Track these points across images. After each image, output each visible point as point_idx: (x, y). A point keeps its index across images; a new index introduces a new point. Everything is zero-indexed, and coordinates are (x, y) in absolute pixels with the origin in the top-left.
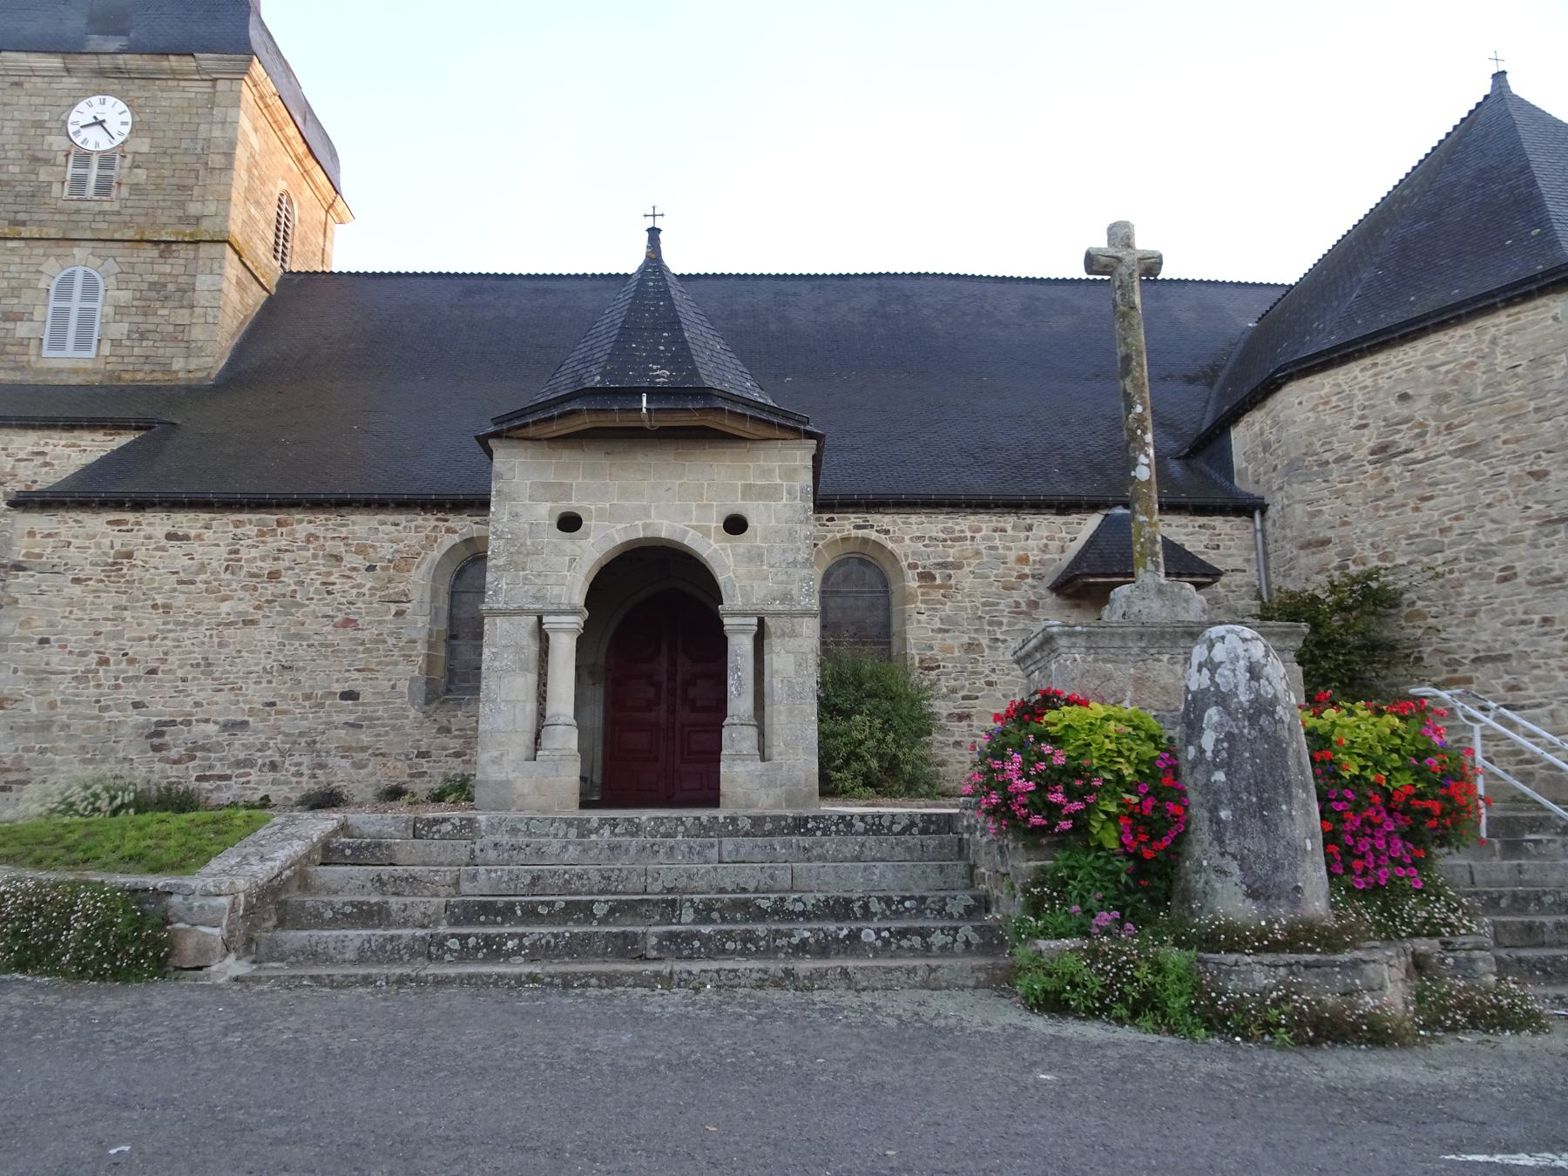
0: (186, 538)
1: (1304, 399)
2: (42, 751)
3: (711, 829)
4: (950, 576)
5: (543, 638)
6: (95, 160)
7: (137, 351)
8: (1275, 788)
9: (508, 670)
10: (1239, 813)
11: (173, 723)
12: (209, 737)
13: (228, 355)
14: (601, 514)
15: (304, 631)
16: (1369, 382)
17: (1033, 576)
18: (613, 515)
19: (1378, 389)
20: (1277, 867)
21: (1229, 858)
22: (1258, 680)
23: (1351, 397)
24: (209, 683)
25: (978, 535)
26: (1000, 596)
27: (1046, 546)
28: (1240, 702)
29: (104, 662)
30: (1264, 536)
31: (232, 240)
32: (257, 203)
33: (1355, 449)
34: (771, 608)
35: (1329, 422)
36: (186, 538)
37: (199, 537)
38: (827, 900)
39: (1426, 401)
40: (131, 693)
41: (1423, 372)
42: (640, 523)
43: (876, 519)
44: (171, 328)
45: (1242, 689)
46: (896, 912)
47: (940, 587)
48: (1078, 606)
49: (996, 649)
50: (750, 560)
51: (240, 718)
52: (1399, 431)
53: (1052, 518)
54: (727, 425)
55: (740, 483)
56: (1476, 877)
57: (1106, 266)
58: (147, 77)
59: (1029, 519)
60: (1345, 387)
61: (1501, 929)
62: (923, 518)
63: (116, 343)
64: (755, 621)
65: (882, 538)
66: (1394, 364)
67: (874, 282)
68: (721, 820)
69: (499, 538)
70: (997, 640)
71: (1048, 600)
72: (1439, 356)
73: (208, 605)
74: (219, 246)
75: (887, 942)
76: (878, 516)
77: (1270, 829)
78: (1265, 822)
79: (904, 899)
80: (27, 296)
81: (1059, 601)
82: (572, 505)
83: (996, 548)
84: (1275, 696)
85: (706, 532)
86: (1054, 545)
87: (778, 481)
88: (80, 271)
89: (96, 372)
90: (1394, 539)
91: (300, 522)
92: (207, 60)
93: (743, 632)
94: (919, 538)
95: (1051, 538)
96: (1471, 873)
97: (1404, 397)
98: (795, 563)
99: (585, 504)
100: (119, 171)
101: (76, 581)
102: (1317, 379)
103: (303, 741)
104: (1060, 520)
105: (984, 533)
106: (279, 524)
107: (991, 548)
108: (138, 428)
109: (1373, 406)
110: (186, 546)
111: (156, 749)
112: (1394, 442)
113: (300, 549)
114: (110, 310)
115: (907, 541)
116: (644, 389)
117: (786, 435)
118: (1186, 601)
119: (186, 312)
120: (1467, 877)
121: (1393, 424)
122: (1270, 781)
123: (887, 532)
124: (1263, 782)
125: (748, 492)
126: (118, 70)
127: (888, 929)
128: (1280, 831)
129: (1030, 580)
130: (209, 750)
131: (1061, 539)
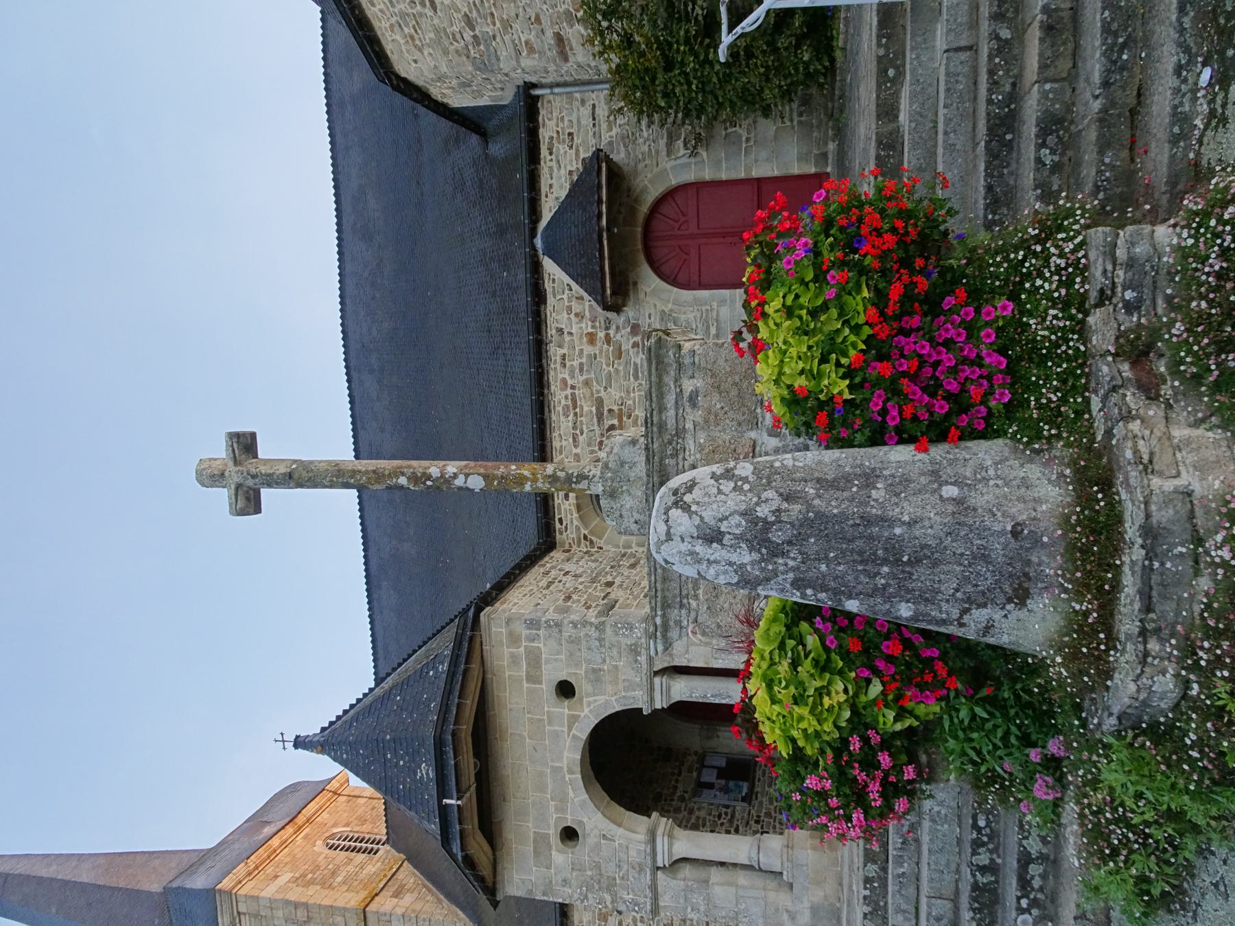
3: (877, 903)
4: (610, 411)
8: (871, 538)
9: (708, 899)
10: (904, 592)
13: (454, 907)
14: (561, 809)
17: (607, 328)
18: (562, 799)
20: (983, 556)
21: (966, 618)
22: (722, 534)
23: (403, 15)
25: (570, 382)
26: (628, 363)
27: (577, 315)
28: (753, 563)
30: (558, 85)
31: (363, 905)
32: (334, 874)
34: (645, 666)
35: (432, 35)
38: (974, 910)
45: (734, 557)
46: (991, 837)
48: (635, 284)
50: (598, 680)
53: (549, 308)
54: (470, 704)
55: (526, 685)
56: (963, 43)
57: (248, 499)
59: (551, 332)
60: (393, 20)
61: (1050, 73)
64: (657, 680)
67: (354, 374)
68: (867, 893)
69: (586, 897)
74: (368, 915)
75: (1034, 903)
77: (926, 556)
78: (918, 561)
79: (975, 826)
81: (631, 303)
82: (553, 834)
83: (581, 364)
84: (743, 514)
85: (573, 720)
86: (576, 307)
87: (522, 649)
93: (669, 690)
94: (574, 440)
96: (958, 49)
98: (600, 640)
99: (552, 822)
102: (389, 47)
104: (551, 300)
107: (581, 370)
116: (440, 801)
117: (478, 644)
118: (622, 464)
120: (963, 56)
122: (859, 543)
124: (861, 553)
125: (533, 678)
127: (1019, 899)
128: (933, 543)
129: (612, 332)
131: (570, 300)
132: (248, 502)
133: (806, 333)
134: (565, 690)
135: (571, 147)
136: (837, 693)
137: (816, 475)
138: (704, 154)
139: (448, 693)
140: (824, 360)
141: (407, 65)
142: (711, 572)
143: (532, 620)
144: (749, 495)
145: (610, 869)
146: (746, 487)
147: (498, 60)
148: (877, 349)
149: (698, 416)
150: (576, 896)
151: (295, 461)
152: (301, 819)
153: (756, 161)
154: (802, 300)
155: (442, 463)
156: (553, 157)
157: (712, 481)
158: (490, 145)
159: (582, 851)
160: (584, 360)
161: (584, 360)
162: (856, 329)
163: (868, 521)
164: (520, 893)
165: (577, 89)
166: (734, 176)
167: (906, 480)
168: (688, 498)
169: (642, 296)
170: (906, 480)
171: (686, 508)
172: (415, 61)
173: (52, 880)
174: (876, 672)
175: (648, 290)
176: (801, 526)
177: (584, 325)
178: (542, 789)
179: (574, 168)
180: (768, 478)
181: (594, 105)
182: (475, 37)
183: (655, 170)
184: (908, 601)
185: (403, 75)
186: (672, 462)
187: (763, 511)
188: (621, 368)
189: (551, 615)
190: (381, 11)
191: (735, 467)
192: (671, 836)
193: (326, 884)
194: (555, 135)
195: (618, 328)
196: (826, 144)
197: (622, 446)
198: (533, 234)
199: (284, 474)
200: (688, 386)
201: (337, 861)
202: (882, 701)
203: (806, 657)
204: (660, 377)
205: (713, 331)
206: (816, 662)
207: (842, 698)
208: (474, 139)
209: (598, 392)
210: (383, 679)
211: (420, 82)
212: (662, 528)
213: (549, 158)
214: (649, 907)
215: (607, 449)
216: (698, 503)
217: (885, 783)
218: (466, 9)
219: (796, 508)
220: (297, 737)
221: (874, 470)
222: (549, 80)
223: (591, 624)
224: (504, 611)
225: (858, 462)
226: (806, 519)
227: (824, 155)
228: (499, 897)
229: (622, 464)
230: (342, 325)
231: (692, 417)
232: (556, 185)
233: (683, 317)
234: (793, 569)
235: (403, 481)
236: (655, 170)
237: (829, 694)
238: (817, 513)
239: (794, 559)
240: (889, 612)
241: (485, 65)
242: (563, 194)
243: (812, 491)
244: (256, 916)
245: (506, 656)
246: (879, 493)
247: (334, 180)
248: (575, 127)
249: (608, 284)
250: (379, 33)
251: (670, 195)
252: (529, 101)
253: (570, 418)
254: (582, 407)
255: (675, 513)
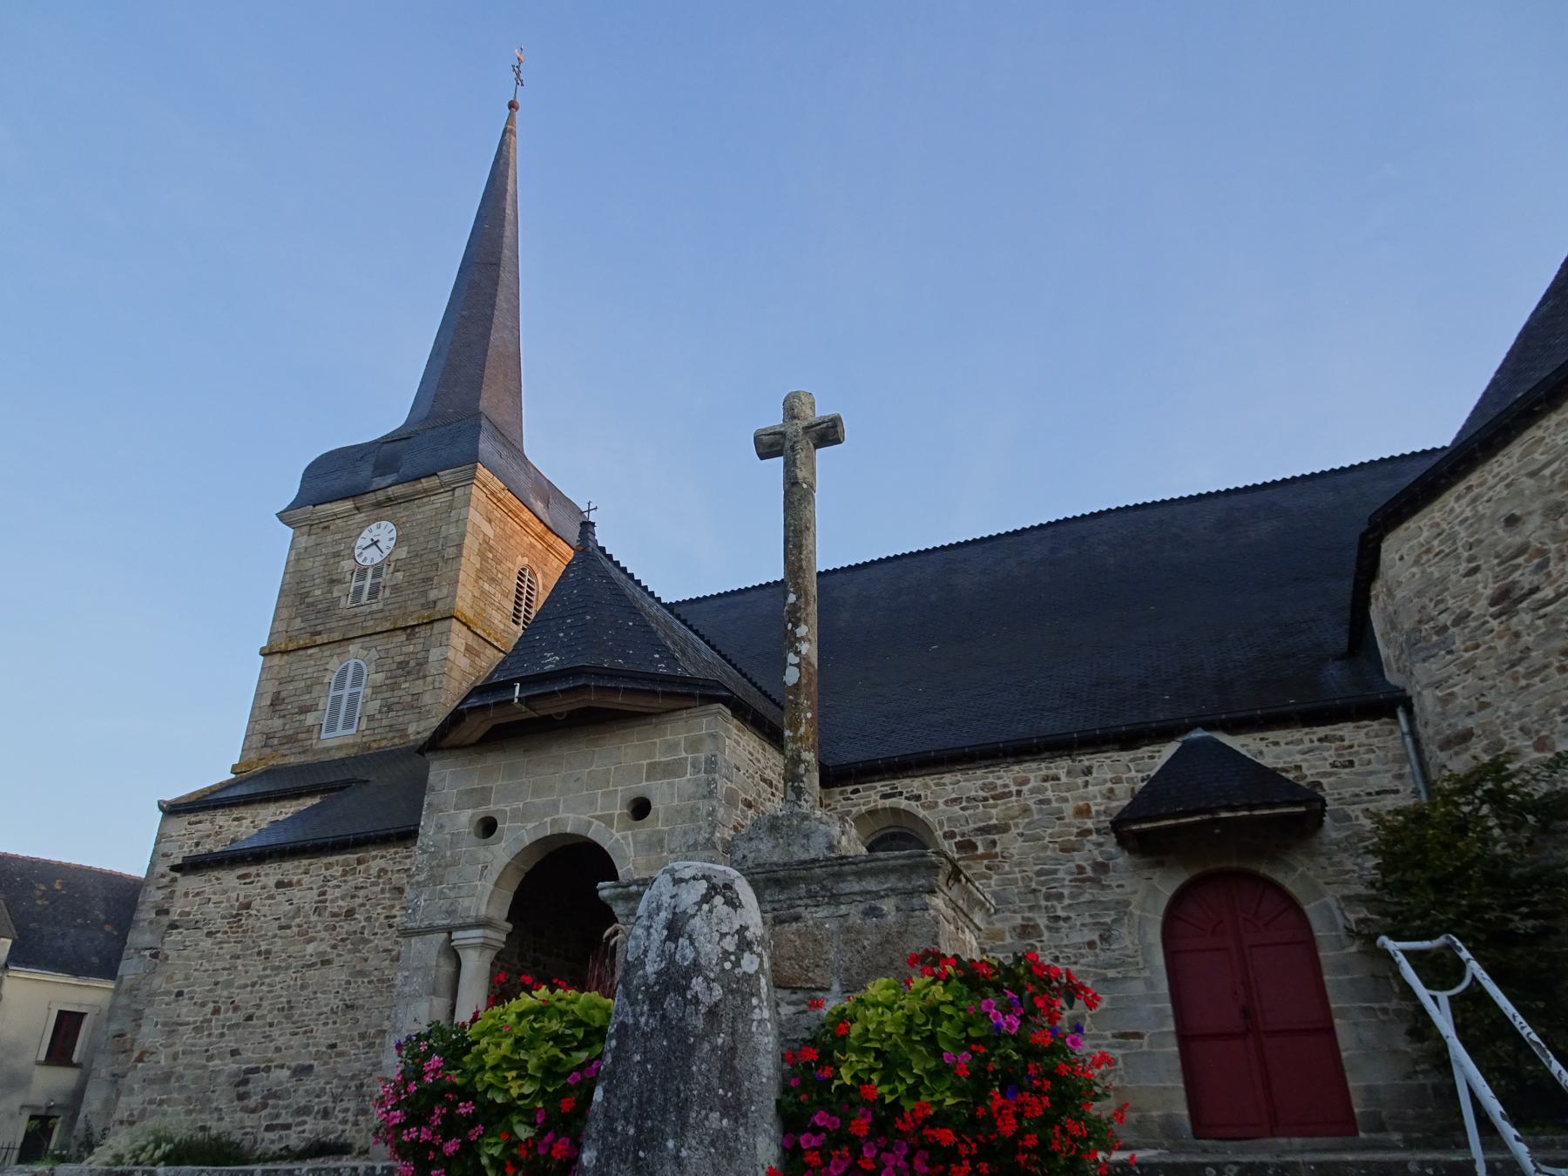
0: (290, 884)
1: (1404, 551)
2: (161, 1102)
4: (994, 843)
5: (453, 955)
6: (370, 572)
7: (385, 722)
8: (664, 1110)
9: (415, 996)
11: (256, 1070)
12: (280, 1083)
15: (368, 967)
16: (1468, 513)
18: (522, 816)
19: (1480, 518)
22: (676, 941)
23: (1453, 537)
24: (288, 1027)
25: (1025, 788)
27: (1111, 790)
28: (645, 976)
29: (216, 1011)
32: (493, 580)
33: (1473, 603)
35: (1437, 575)
36: (290, 884)
37: (299, 882)
39: (1536, 520)
40: (230, 1042)
41: (1528, 483)
42: (548, 820)
43: (914, 784)
44: (409, 698)
45: (651, 955)
47: (983, 857)
48: (1160, 864)
49: (1058, 930)
51: (307, 1063)
52: (1517, 567)
53: (1115, 755)
54: (619, 702)
57: (772, 445)
58: (408, 499)
59: (1086, 761)
60: (1444, 526)
62: (959, 776)
63: (371, 718)
65: (913, 806)
66: (1491, 481)
67: (1050, 531)
69: (425, 852)
70: (1057, 918)
71: (1120, 860)
72: (1539, 457)
73: (297, 948)
74: (447, 622)
76: (907, 781)
80: (317, 690)
82: (490, 809)
83: (1048, 801)
84: (695, 963)
85: (608, 820)
87: (684, 755)
88: (352, 662)
89: (354, 745)
90: (1546, 717)
91: (374, 858)
92: (446, 475)
95: (1117, 780)
97: (1512, 521)
99: (501, 806)
100: (386, 576)
101: (209, 934)
102: (1411, 524)
103: (353, 1084)
104: (1126, 756)
105: (1032, 784)
106: (359, 862)
107: (1041, 802)
108: (322, 792)
109: (1480, 541)
110: (289, 892)
111: (241, 1097)
112: (1514, 583)
113: (373, 884)
114: (369, 691)
115: (942, 806)
116: (516, 680)
118: (807, 836)
119: (420, 682)
121: (1507, 560)
122: (660, 1099)
123: (918, 798)
124: (650, 1101)
125: (654, 771)
126: (389, 499)
129: (1094, 837)
130: (279, 1098)
132: (768, 446)
133: (908, 1032)
134: (641, 808)
135: (1333, 765)
136: (520, 1086)
137: (740, 1047)
138: (1353, 949)
139: (632, 676)
140: (879, 1054)
141: (1397, 551)
142: (639, 931)
143: (715, 763)
144: (717, 969)
145: (452, 878)
146: (728, 965)
147: (1424, 660)
148: (886, 1118)
149: (856, 920)
150: (426, 841)
151: (812, 487)
152: (551, 538)
153: (1356, 1024)
154: (945, 1024)
155: (814, 638)
156: (1316, 744)
157: (737, 927)
158: (1338, 663)
159: (469, 844)
160: (1055, 804)
161: (1055, 804)
162: (913, 1092)
163: (683, 1108)
164: (432, 778)
165: (1416, 768)
166: (1330, 992)
167: (731, 1155)
168: (718, 900)
169: (1146, 874)
170: (731, 1156)
171: (706, 898)
172: (1401, 558)
173: (493, 306)
174: (541, 1133)
175: (1155, 882)
176: (681, 1029)
177: (1099, 800)
178: (536, 792)
179: (1305, 771)
180: (738, 991)
181: (1396, 792)
182: (1445, 628)
183: (1321, 881)
184: (598, 1159)
185: (1384, 546)
186: (803, 892)
187: (697, 984)
188: (1049, 853)
189: (723, 786)
190: (1452, 510)
191: (752, 952)
192: (484, 946)
193: (482, 573)
194: (1346, 743)
195: (1100, 845)
196: (1397, 1129)
197: (827, 835)
198: (1208, 726)
199: (796, 477)
200: (887, 905)
201: (506, 582)
202: (513, 1142)
203: (563, 1051)
204: (893, 870)
205: (1111, 973)
206: (555, 1061)
207: (514, 1092)
208: (1344, 642)
209: (1016, 825)
210: (671, 612)
211: (1382, 568)
212: (687, 874)
213: (1315, 738)
214: (410, 925)
215: (825, 818)
216: (711, 911)
217: (428, 1145)
218: (1476, 613)
219: (700, 1023)
220: (593, 524)
221: (745, 1116)
222: (1420, 728)
223: (712, 833)
224: (728, 729)
225: (755, 1098)
226: (687, 1035)
227: (1380, 1127)
228: (428, 756)
229: (807, 836)
230: (1109, 510)
231: (854, 912)
232: (1276, 750)
233: (1124, 931)
234: (637, 1023)
235: (792, 598)
236: (1321, 881)
237: (518, 1077)
238: (692, 1047)
239: (647, 1023)
240: (589, 1137)
241: (1414, 644)
242: (1267, 761)
243: (720, 1041)
244: (451, 508)
245: (677, 737)
246: (716, 1121)
247: (1294, 478)
248: (1363, 769)
249: (1144, 826)
250: (1426, 510)
251: (1291, 904)
252: (1387, 704)
253: (981, 793)
254: (995, 806)
255: (702, 886)
